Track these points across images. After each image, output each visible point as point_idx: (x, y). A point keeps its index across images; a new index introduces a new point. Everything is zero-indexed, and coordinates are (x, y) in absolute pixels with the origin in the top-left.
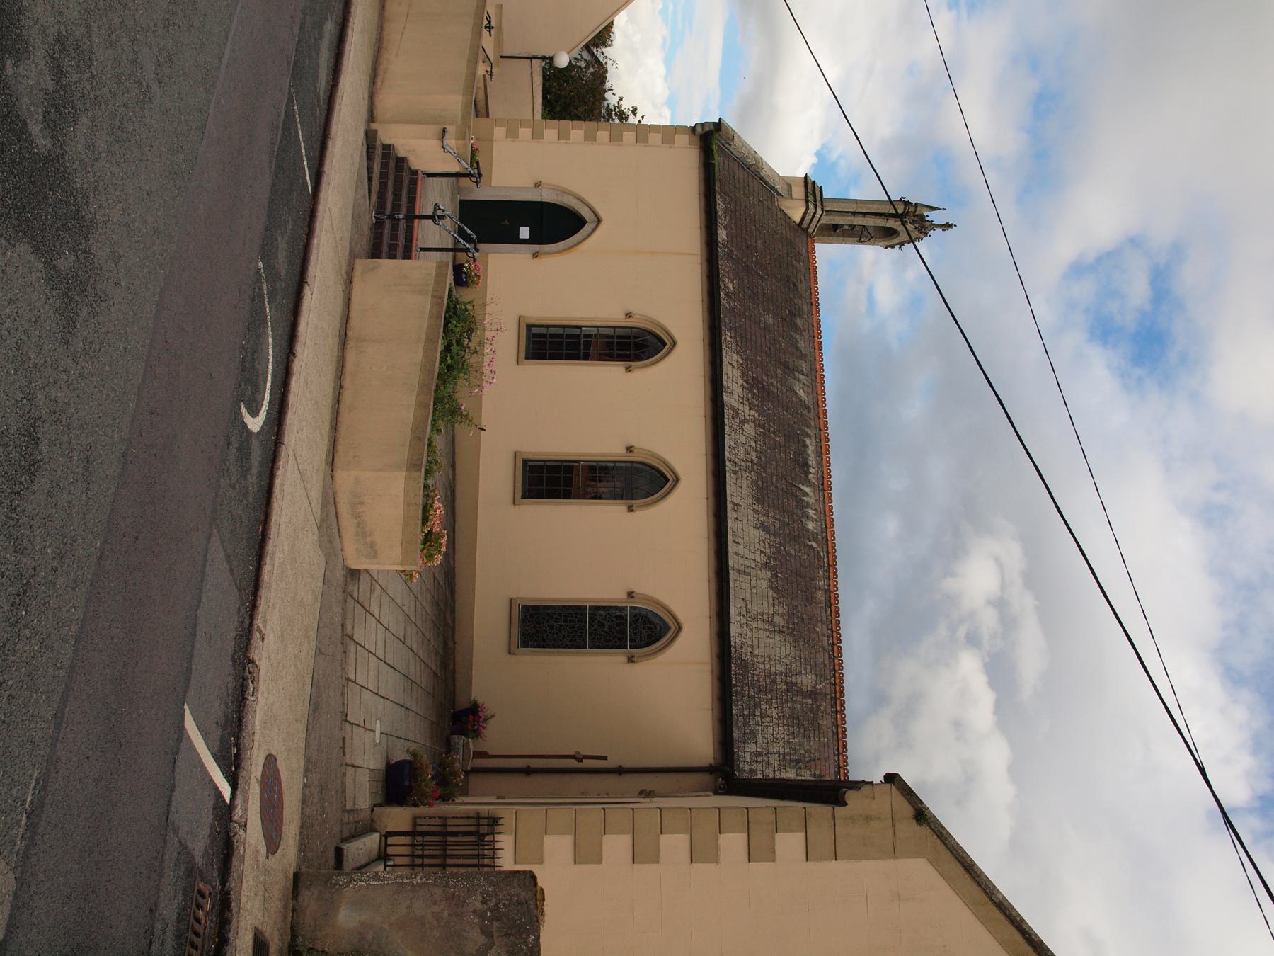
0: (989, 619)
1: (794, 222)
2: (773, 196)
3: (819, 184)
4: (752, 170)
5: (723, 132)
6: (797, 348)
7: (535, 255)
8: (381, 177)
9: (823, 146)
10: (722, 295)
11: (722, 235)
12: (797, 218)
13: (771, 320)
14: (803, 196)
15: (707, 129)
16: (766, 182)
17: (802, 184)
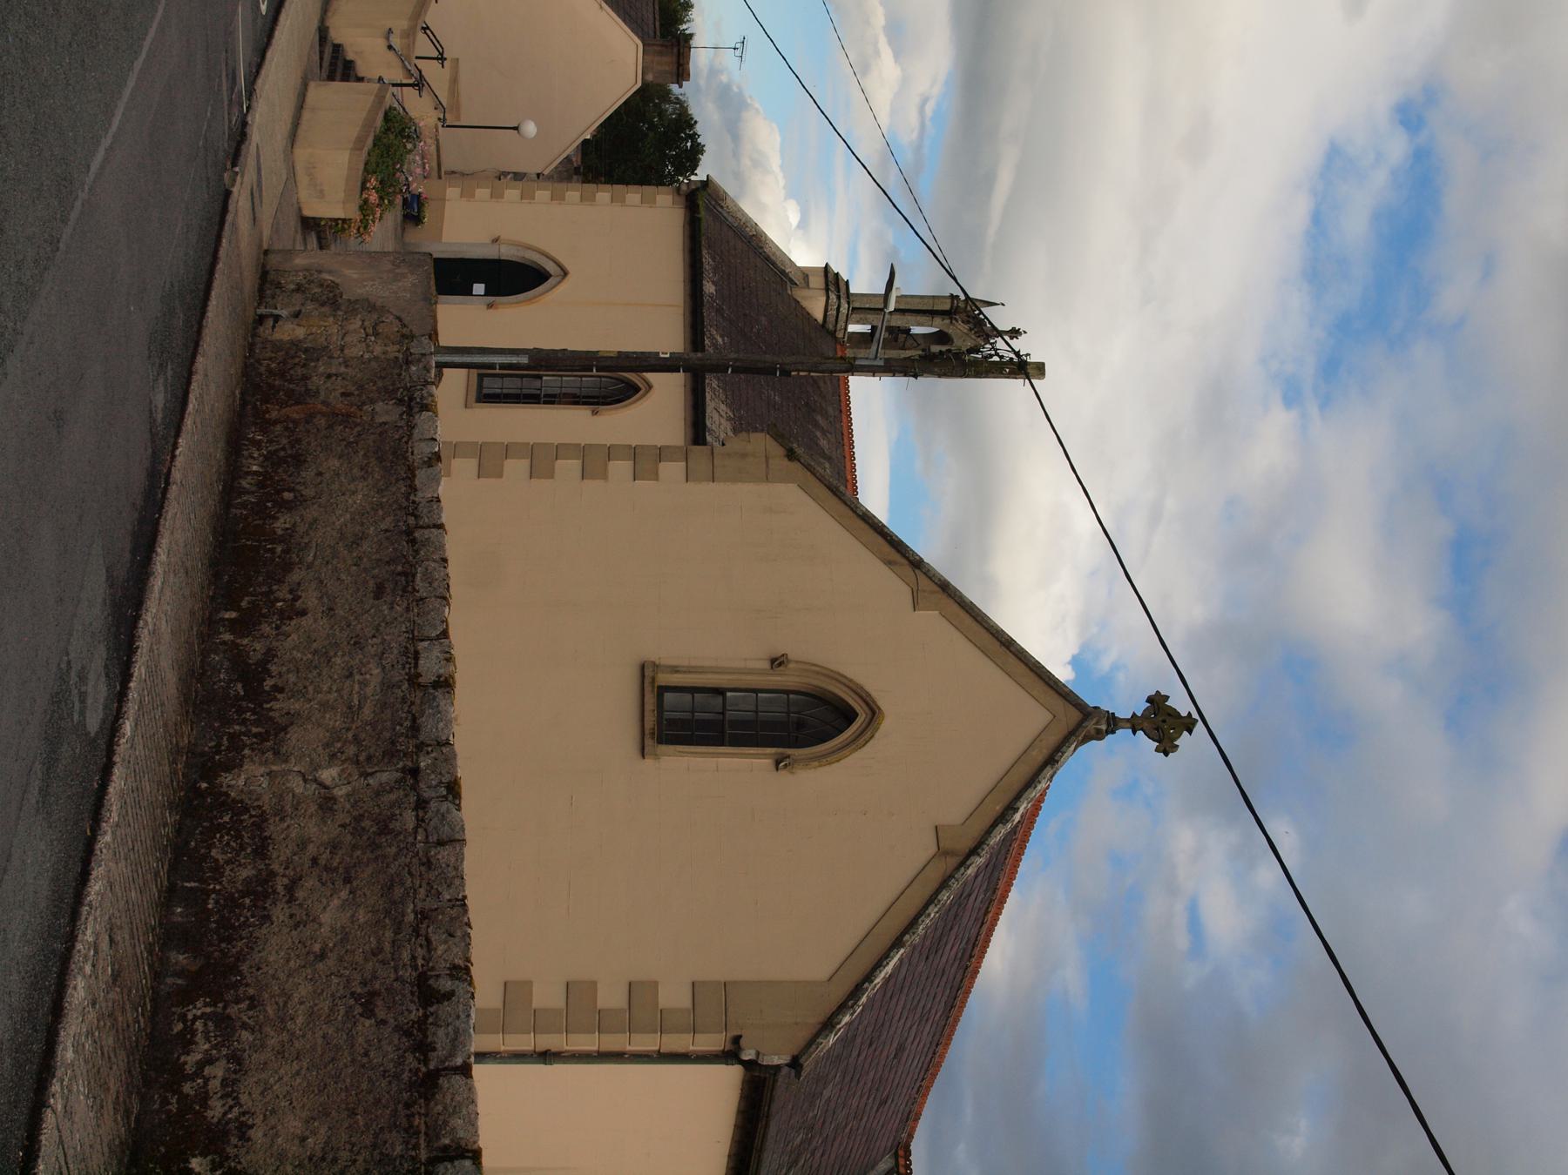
1: (816, 320)
2: (783, 284)
3: (845, 277)
4: (752, 244)
5: (711, 185)
6: (817, 445)
7: (490, 306)
9: (1085, 647)
10: (707, 342)
11: (709, 288)
12: (819, 316)
13: (777, 398)
14: (823, 286)
15: (693, 187)
16: (774, 264)
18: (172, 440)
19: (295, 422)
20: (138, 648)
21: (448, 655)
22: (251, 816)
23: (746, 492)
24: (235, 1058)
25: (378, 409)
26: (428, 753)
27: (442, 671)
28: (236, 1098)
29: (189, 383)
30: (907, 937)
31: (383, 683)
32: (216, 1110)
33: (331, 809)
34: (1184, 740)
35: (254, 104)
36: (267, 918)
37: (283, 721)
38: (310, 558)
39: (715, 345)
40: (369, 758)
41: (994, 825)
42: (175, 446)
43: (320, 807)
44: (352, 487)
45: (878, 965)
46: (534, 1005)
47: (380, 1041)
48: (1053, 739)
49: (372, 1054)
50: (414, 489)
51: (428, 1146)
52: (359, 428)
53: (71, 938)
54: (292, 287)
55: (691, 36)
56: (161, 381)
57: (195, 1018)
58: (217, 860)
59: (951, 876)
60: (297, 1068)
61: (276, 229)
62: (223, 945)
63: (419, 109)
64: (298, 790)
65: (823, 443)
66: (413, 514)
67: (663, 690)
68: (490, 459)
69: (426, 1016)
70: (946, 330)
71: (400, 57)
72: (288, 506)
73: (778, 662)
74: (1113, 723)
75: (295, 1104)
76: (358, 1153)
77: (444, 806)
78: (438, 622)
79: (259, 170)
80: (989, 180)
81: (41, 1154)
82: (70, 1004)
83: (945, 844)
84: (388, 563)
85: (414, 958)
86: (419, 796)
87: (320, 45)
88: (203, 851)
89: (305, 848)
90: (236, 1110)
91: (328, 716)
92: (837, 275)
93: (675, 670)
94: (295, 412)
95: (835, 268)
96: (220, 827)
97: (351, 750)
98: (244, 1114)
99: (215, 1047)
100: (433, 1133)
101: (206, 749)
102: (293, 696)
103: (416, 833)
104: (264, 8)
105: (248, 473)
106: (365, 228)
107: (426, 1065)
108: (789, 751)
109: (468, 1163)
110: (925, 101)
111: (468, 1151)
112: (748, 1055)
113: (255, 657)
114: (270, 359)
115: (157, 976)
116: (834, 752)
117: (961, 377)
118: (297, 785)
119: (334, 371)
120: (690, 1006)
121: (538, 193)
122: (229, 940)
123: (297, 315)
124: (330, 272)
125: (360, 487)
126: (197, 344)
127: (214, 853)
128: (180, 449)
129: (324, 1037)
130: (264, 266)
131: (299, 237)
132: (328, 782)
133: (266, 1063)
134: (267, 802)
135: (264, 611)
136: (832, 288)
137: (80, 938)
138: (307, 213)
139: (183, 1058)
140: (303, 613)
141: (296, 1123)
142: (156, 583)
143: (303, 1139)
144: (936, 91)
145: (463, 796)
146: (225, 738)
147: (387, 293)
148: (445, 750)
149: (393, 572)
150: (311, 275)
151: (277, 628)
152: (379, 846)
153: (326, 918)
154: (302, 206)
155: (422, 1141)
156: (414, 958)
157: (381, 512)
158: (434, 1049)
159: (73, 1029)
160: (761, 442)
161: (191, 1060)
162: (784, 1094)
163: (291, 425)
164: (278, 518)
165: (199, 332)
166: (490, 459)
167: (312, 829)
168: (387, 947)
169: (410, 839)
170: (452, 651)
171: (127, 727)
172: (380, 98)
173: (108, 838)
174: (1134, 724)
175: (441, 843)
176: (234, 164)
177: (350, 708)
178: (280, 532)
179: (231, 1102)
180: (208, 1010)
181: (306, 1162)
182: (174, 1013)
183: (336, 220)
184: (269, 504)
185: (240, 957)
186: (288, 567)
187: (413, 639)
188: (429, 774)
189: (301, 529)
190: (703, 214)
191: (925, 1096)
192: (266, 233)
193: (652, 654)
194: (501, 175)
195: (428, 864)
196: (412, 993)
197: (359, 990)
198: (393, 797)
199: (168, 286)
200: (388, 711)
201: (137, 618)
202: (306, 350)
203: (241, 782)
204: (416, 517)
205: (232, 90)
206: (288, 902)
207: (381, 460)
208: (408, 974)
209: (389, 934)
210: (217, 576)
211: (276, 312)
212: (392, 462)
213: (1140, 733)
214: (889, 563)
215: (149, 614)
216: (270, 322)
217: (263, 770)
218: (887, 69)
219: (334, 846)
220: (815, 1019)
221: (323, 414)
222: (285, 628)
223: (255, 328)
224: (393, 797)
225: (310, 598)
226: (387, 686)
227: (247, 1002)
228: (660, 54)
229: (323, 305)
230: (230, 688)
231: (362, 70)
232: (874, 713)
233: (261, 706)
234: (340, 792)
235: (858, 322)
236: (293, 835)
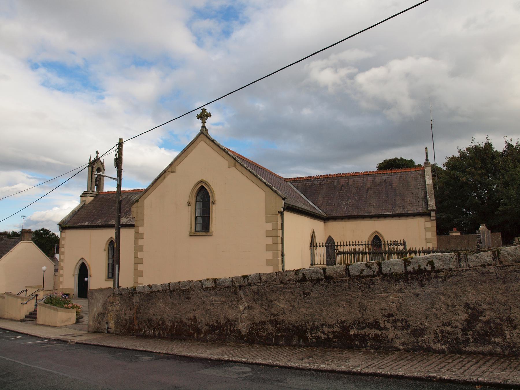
0: (343, 72)
2: (85, 207)
4: (75, 214)
6: (125, 198)
7: (91, 276)
8: (31, 318)
10: (100, 224)
11: (86, 224)
12: (92, 198)
15: (60, 228)
16: (80, 209)
17: (82, 197)
18: (155, 354)
19: (139, 322)
20: (219, 359)
21: (207, 280)
22: (254, 326)
23: (147, 211)
24: (322, 326)
25: (135, 301)
26: (235, 284)
27: (211, 281)
28: (333, 324)
29: (136, 350)
30: (255, 174)
31: (215, 296)
32: (337, 329)
33: (251, 307)
34: (208, 111)
35: (48, 337)
36: (283, 321)
37: (226, 320)
38: (179, 316)
39: (101, 222)
40: (237, 298)
41: (228, 154)
42: (156, 353)
43: (251, 309)
44: (158, 307)
45: (261, 180)
46: (272, 258)
47: (317, 291)
48: (208, 140)
49: (320, 292)
50: (158, 291)
51: (345, 277)
52: (141, 306)
53: (310, 370)
54: (99, 324)
55: (13, 232)
56: (142, 358)
57: (311, 336)
58: (267, 334)
59: (241, 164)
60: (325, 310)
61: (81, 330)
62: (291, 331)
63: (41, 295)
64: (246, 315)
65: (124, 197)
66: (166, 291)
67: (196, 231)
68: (138, 274)
69: (309, 280)
70: (96, 169)
71: (29, 301)
72: (163, 323)
73: (189, 204)
74: (204, 127)
75: (335, 310)
76: (348, 294)
77: (250, 278)
78: (197, 283)
79: (67, 335)
80: (48, 163)
81: (375, 372)
82: (329, 368)
83: (233, 165)
84: (180, 296)
85: (293, 284)
86: (247, 285)
87: (25, 321)
88: (264, 338)
89: (263, 312)
90: (337, 324)
91: (225, 309)
92: (82, 194)
93: (191, 228)
94: (136, 322)
95: (81, 194)
96: (257, 334)
97: (234, 303)
98: (338, 323)
99: (319, 331)
100: (342, 276)
101: (235, 339)
102: (219, 318)
103: (258, 285)
104: (19, 337)
105: (154, 333)
106: (78, 307)
107: (323, 279)
108: (211, 201)
109: (350, 267)
110: (28, 178)
111: (346, 267)
112: (282, 210)
113: (208, 328)
114: (120, 329)
115: (300, 347)
116: (211, 192)
117: (122, 159)
118: (244, 316)
119: (124, 313)
120: (271, 223)
121: (61, 266)
122: (289, 330)
123: (107, 323)
124: (95, 315)
125: (158, 304)
126: (124, 349)
127: (264, 335)
128: (157, 351)
129: (316, 304)
130: (92, 332)
131: (81, 324)
132: (244, 308)
133: (324, 318)
134: (249, 322)
135: (194, 326)
136: (86, 195)
137: (310, 368)
138: (75, 322)
139: (323, 338)
140: (195, 317)
141: (340, 309)
142: (199, 355)
143: (344, 307)
144: (26, 175)
145: (246, 274)
146: (231, 334)
147: (101, 300)
148: (234, 279)
149: (183, 295)
150: (95, 320)
151: (199, 323)
152: (262, 294)
153: (282, 306)
154: (73, 323)
155: (344, 279)
156: (293, 284)
157: (165, 299)
158: (319, 277)
159: (334, 366)
160: (134, 209)
161: (323, 336)
162: (292, 202)
163: (140, 323)
164: (167, 325)
165: (119, 348)
166: (138, 274)
167: (257, 311)
168: (290, 290)
169: (260, 286)
170: (206, 279)
171: (244, 360)
172: (42, 305)
173: (278, 362)
174: (203, 122)
175: (261, 279)
176: (68, 342)
177: (222, 303)
178: (171, 324)
179: (335, 326)
180: (309, 333)
181: (351, 306)
182: (310, 341)
183: (76, 314)
184: (163, 327)
185: (294, 326)
186: (181, 321)
187: (202, 289)
188: (241, 283)
189: (170, 319)
190: (67, 225)
191: (276, 174)
192: (83, 332)
193: (187, 233)
194: (55, 275)
195: (266, 282)
196: (303, 284)
197: (303, 297)
198: (248, 292)
199: (113, 358)
200: (223, 294)
201: (210, 360)
202: (118, 320)
203: (244, 329)
204: (166, 290)
205: (46, 344)
206: (278, 315)
207: (150, 299)
208: (298, 285)
209: (287, 290)
210: (184, 339)
211: (106, 328)
212: (150, 297)
213: (206, 121)
214: (164, 178)
215: (209, 356)
216: (109, 330)
217: (240, 324)
218: (20, 186)
219: (262, 305)
220: (274, 195)
221: (137, 315)
222: (199, 321)
223: (111, 333)
224: (248, 292)
225: (191, 315)
226: (216, 295)
227: (306, 324)
228: (24, 237)
229: (104, 317)
230: (217, 334)
231: (32, 310)
232: (201, 182)
233: (222, 326)
234: (246, 305)
235: (94, 189)
236: (259, 315)
